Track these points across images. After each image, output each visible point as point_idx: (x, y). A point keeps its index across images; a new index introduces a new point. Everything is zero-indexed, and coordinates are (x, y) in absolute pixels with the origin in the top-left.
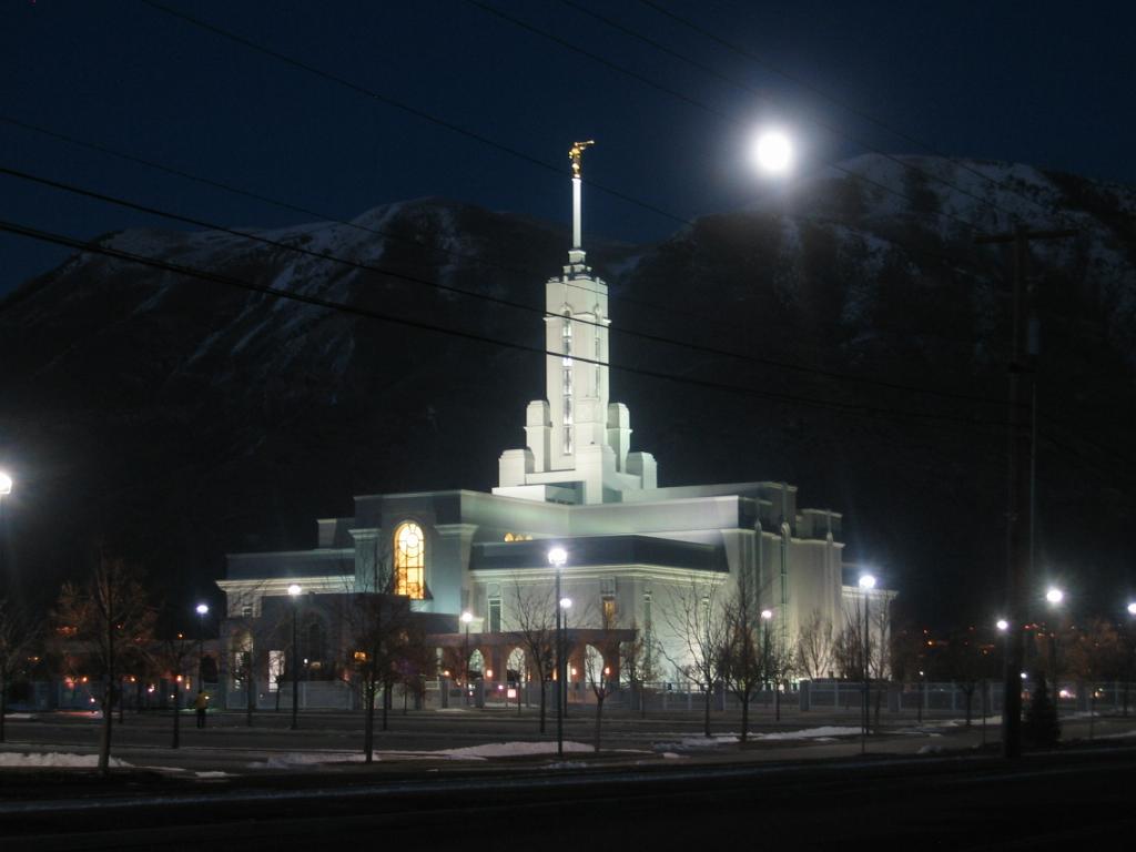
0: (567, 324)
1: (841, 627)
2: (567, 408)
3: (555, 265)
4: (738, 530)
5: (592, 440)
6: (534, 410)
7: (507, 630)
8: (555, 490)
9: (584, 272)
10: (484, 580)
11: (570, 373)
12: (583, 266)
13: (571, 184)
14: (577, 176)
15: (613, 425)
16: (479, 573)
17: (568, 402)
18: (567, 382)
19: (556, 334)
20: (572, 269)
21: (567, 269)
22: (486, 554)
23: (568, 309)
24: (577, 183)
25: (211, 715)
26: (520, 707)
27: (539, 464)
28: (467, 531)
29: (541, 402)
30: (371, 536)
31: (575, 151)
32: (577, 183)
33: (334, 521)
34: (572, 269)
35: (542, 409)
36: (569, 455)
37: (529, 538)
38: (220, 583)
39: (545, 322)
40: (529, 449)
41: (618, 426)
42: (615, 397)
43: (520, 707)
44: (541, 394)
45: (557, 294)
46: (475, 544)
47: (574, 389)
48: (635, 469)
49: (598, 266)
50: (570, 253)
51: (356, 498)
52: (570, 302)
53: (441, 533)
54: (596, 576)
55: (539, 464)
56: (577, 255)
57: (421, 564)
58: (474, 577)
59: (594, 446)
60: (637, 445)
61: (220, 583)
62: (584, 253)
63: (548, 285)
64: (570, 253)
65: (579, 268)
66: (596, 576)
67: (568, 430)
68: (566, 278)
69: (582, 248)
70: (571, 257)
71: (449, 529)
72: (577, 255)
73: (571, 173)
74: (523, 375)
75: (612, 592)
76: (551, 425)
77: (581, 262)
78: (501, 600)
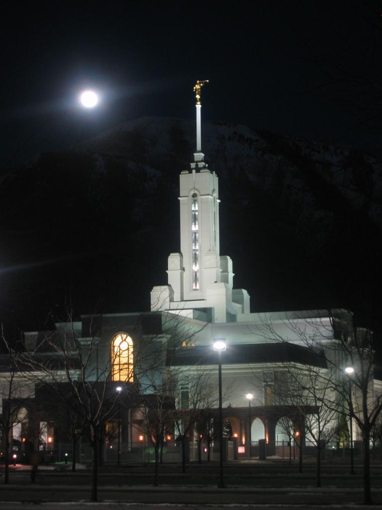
0: (195, 202)
2: (195, 259)
3: (185, 163)
4: (334, 340)
5: (215, 280)
6: (173, 260)
8: (198, 312)
9: (204, 167)
11: (197, 235)
12: (204, 163)
13: (195, 108)
14: (199, 103)
15: (225, 270)
17: (196, 254)
18: (195, 241)
19: (187, 207)
20: (197, 165)
21: (193, 165)
23: (196, 192)
24: (199, 107)
25: (154, 460)
26: (290, 459)
27: (177, 296)
28: (164, 339)
29: (178, 254)
31: (197, 87)
32: (199, 107)
33: (36, 333)
34: (197, 165)
35: (179, 259)
36: (196, 290)
37: (193, 345)
39: (179, 200)
40: (169, 286)
41: (228, 272)
42: (223, 252)
43: (290, 459)
44: (177, 249)
45: (187, 182)
47: (200, 247)
48: (239, 301)
49: (212, 164)
50: (195, 154)
52: (196, 187)
55: (177, 296)
56: (199, 156)
57: (131, 361)
59: (216, 284)
60: (238, 284)
62: (203, 155)
64: (195, 154)
65: (201, 165)
67: (196, 275)
68: (194, 171)
69: (202, 151)
70: (195, 157)
72: (199, 156)
73: (195, 101)
74: (162, 236)
76: (183, 269)
77: (202, 161)
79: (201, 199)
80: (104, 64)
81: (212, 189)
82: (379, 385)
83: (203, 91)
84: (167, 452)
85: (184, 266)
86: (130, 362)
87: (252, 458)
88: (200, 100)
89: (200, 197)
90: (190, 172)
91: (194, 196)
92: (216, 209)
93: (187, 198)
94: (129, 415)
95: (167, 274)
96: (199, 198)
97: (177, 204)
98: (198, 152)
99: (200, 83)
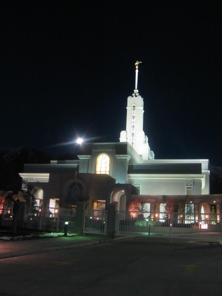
1: (145, 209)
7: (203, 194)
10: (133, 178)
16: (132, 175)
22: (134, 168)
24: (137, 71)
30: (88, 158)
31: (136, 63)
32: (137, 71)
38: (20, 174)
46: (129, 164)
51: (24, 176)
53: (118, 158)
54: (185, 179)
56: (136, 91)
58: (129, 177)
61: (20, 174)
63: (128, 98)
66: (185, 179)
71: (122, 157)
72: (136, 91)
73: (136, 69)
75: (191, 185)
76: (127, 138)
78: (141, 186)
79: (137, 108)
80: (82, 132)
81: (142, 105)
82: (133, 177)
83: (139, 65)
84: (155, 226)
85: (127, 137)
86: (193, 219)
87: (140, 180)
88: (138, 69)
89: (137, 107)
90: (133, 97)
91: (134, 107)
92: (142, 115)
93: (130, 107)
94: (111, 197)
95: (126, 110)
96: (136, 108)
97: (125, 111)
98: (136, 89)
99: (138, 62)
